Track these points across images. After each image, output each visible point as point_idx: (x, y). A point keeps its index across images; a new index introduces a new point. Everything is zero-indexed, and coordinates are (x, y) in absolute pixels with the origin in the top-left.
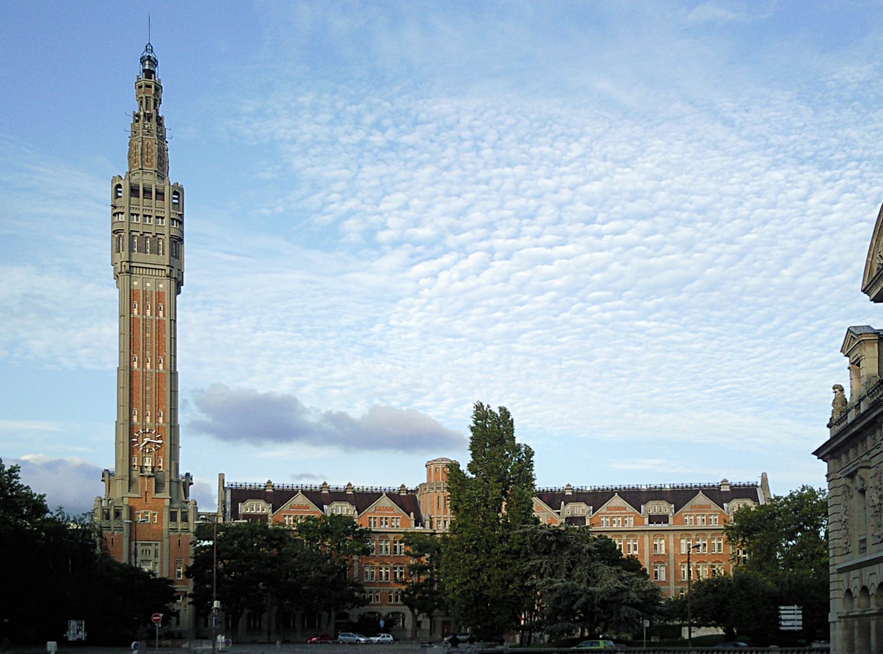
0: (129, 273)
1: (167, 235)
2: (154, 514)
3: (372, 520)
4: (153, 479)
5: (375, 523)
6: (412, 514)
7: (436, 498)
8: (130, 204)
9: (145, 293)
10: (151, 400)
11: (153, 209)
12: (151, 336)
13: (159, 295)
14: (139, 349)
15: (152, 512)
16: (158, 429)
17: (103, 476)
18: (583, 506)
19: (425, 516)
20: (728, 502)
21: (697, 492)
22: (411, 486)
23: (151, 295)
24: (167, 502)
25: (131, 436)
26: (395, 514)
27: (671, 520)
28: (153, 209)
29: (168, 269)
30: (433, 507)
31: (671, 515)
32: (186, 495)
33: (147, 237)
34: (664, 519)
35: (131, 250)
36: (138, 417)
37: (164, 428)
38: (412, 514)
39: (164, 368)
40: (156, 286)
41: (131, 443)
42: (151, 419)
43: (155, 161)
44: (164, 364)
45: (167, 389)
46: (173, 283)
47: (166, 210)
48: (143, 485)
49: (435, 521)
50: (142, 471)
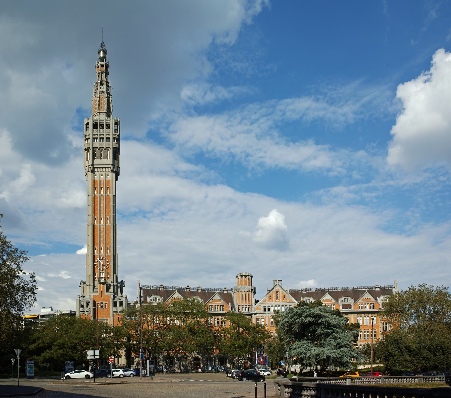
0: (93, 171)
1: (112, 148)
2: (106, 304)
3: (216, 307)
4: (105, 285)
5: (218, 308)
6: (230, 303)
7: (241, 295)
8: (93, 133)
9: (100, 181)
10: (103, 241)
11: (105, 134)
12: (103, 205)
13: (107, 182)
14: (97, 213)
15: (104, 302)
16: (107, 256)
17: (80, 284)
18: (350, 298)
19: (236, 305)
20: (379, 297)
21: (364, 292)
22: (229, 288)
23: (103, 182)
24: (112, 297)
25: (94, 261)
26: (333, 303)
27: (352, 307)
28: (105, 134)
29: (112, 167)
30: (239, 299)
31: (352, 304)
32: (122, 292)
33: (102, 150)
34: (349, 306)
35: (94, 158)
36: (97, 251)
37: (110, 256)
38: (230, 303)
39: (110, 223)
40: (106, 177)
41: (94, 265)
42: (103, 252)
43: (105, 107)
44: (110, 220)
45: (111, 234)
46: (114, 174)
47: (111, 134)
48: (100, 288)
49: (241, 307)
50: (99, 281)
